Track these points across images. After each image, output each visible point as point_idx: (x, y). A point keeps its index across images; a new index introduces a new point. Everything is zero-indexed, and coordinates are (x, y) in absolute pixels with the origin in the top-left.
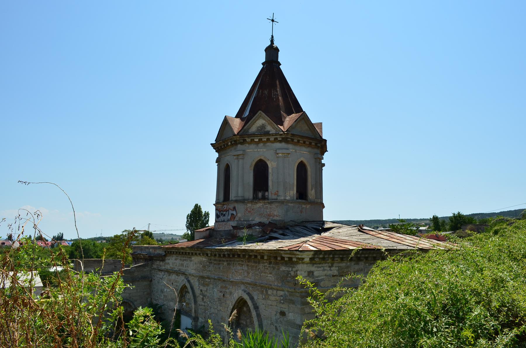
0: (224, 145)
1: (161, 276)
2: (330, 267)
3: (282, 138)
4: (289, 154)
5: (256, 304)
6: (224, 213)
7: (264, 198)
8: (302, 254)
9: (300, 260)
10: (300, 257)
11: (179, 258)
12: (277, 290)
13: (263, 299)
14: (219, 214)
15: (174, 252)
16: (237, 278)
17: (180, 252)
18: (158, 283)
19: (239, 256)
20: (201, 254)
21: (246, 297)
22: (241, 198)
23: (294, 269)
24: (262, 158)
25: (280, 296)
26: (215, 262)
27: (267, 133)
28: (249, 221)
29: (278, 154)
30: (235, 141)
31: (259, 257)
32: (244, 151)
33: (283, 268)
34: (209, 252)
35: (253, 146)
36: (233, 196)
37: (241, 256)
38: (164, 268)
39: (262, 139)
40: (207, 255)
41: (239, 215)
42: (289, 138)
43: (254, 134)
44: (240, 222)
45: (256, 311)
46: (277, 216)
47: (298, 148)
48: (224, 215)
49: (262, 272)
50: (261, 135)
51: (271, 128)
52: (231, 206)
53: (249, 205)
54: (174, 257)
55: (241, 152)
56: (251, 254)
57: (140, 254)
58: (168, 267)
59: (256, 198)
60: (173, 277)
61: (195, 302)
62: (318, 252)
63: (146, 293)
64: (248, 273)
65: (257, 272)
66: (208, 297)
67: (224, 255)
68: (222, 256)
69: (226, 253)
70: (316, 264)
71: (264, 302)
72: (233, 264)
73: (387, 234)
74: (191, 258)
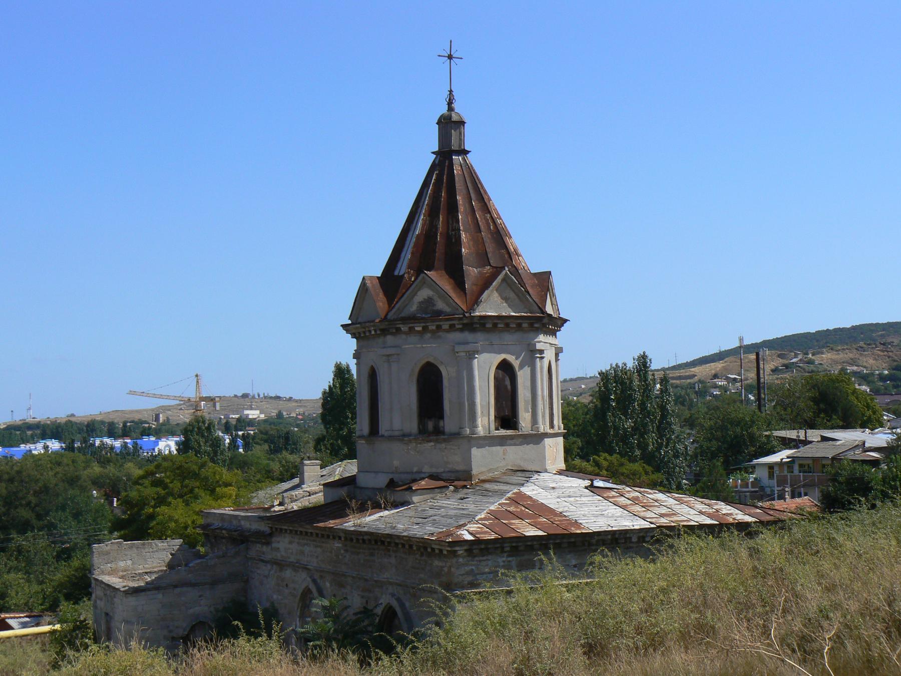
11: (296, 540)
15: (286, 530)
17: (296, 531)
19: (383, 543)
21: (395, 604)
22: (397, 433)
23: (448, 564)
24: (431, 360)
31: (407, 547)
35: (413, 338)
38: (270, 557)
40: (340, 538)
59: (423, 431)
62: (478, 542)
69: (365, 538)
70: (475, 556)
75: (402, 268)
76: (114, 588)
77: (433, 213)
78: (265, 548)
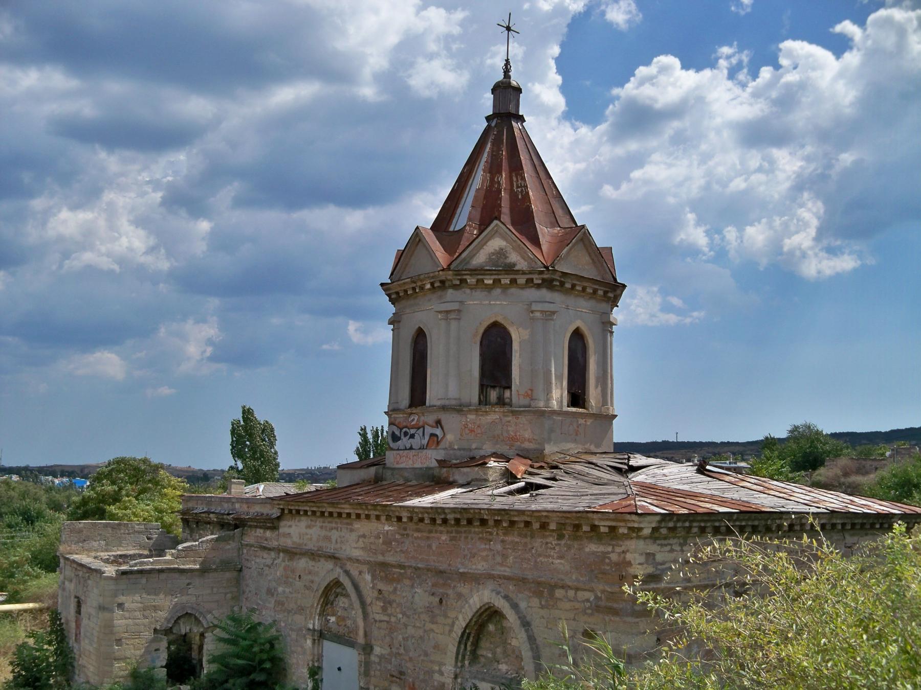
0: (414, 289)
1: (269, 562)
2: (681, 545)
3: (543, 280)
4: (554, 313)
5: (525, 617)
6: (412, 431)
7: (501, 402)
8: (641, 519)
9: (633, 531)
10: (636, 525)
12: (577, 589)
13: (542, 607)
14: (397, 433)
15: (306, 512)
16: (479, 566)
17: (323, 513)
18: (260, 574)
19: (483, 522)
20: (383, 518)
21: (501, 604)
22: (453, 402)
24: (500, 319)
25: (583, 602)
26: (419, 535)
27: (510, 269)
28: (470, 450)
29: (532, 312)
30: (443, 282)
32: (461, 302)
33: (592, 547)
34: (405, 515)
35: (478, 294)
36: (434, 393)
37: (491, 523)
39: (500, 280)
41: (450, 437)
42: (556, 280)
43: (482, 270)
44: (451, 452)
45: (527, 631)
46: (529, 441)
47: (571, 300)
48: (412, 436)
49: (540, 555)
50: (498, 272)
51: (519, 258)
52: (431, 418)
53: (471, 417)
54: (304, 522)
55: (455, 306)
56: (516, 519)
57: (209, 513)
58: (288, 543)
59: (484, 401)
60: (303, 563)
61: (365, 615)
63: (229, 596)
64: (505, 556)
65: (528, 556)
66: (399, 605)
67: (445, 521)
68: (439, 521)
71: (544, 612)
72: (466, 538)
73: (756, 481)
74: (351, 524)
75: (461, 221)
76: (90, 568)
77: (494, 169)
78: (268, 533)
